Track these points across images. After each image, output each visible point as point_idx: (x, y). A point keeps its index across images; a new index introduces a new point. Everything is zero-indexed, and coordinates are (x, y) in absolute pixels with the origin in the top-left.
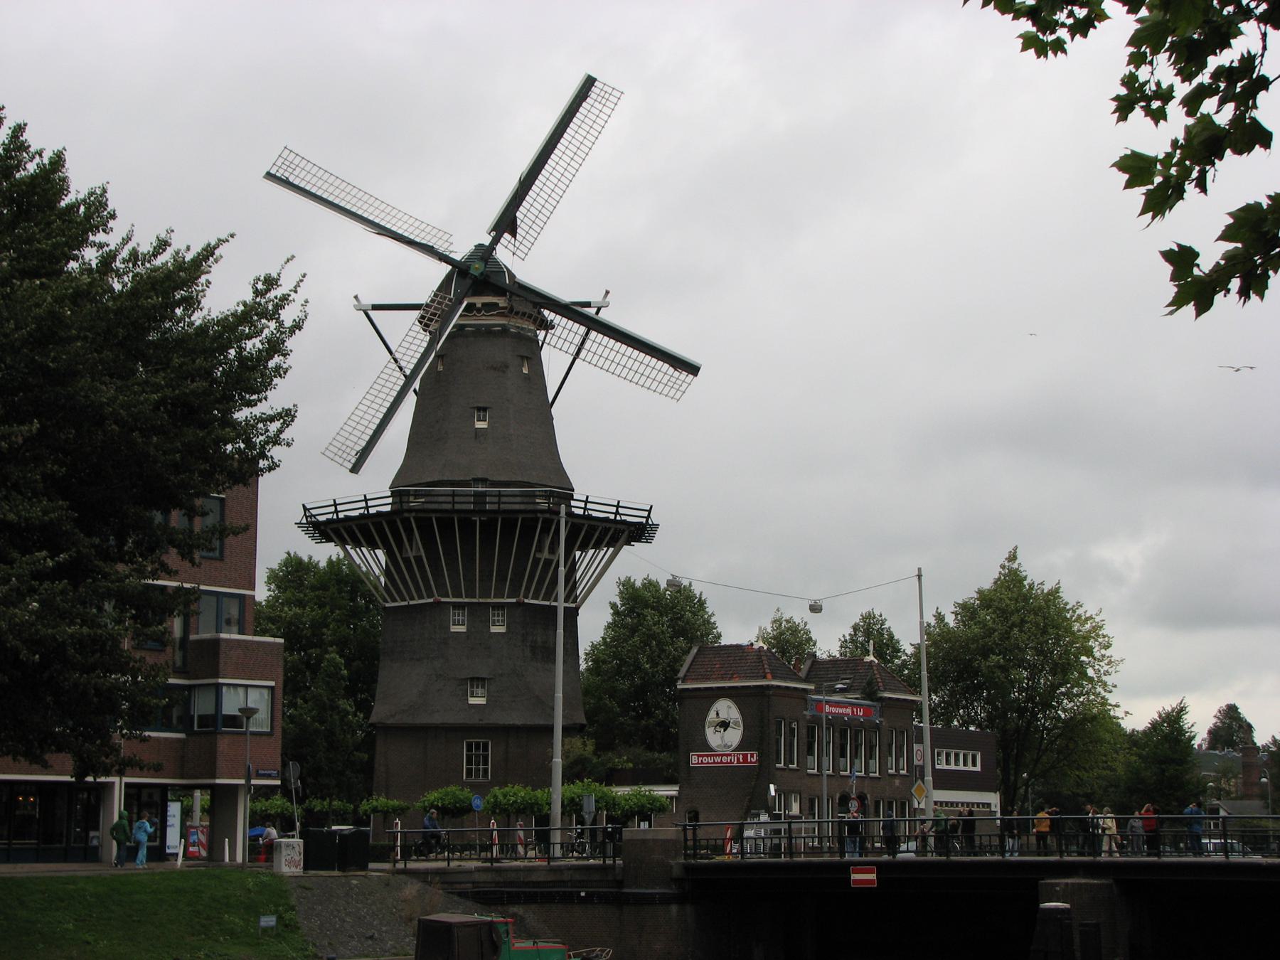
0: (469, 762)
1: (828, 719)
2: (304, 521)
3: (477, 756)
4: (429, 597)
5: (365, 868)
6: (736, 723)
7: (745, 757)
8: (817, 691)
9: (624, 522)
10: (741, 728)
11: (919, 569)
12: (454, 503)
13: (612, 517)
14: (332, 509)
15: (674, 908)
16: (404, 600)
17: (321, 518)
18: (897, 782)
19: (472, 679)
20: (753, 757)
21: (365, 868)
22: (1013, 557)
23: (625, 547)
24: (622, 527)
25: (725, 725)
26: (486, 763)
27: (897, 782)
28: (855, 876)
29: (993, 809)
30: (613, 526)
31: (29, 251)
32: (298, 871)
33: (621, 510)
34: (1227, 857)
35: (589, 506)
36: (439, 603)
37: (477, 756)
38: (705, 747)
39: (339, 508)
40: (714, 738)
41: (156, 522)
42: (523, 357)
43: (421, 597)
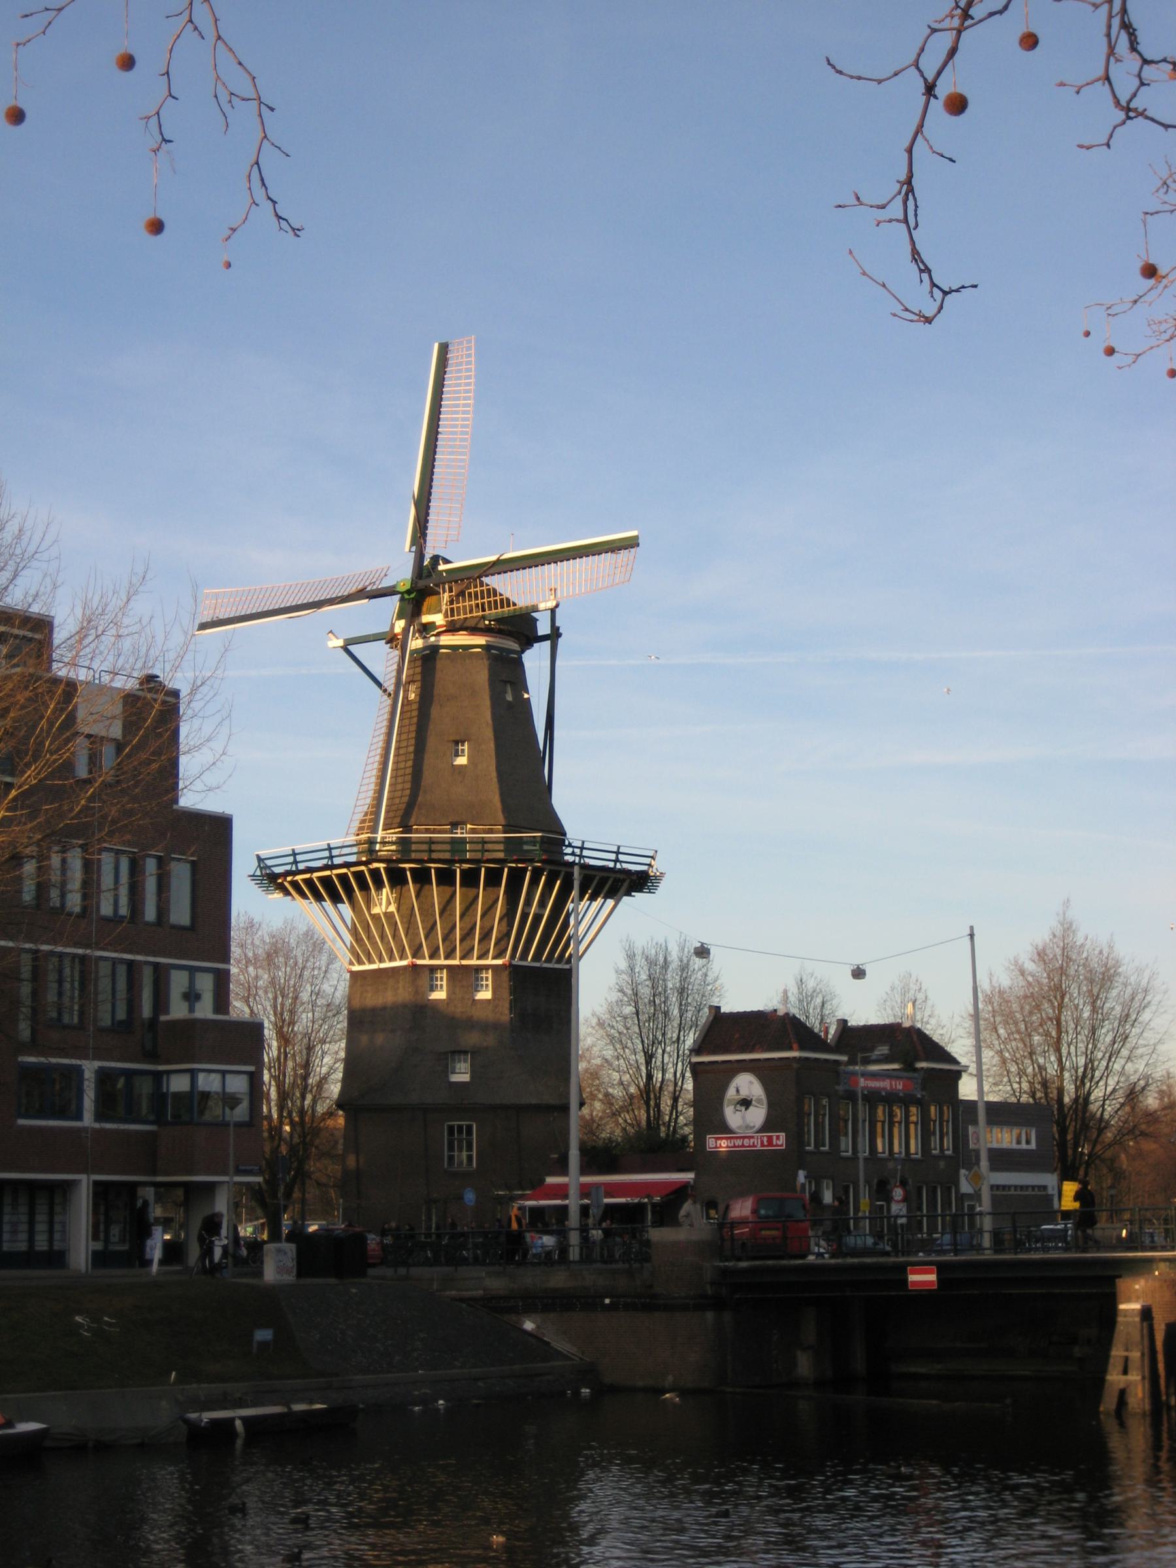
0: (451, 1148)
1: (863, 1095)
2: (258, 873)
3: (460, 1141)
4: (401, 959)
5: (364, 1275)
6: (759, 1101)
7: (770, 1139)
8: (852, 1062)
9: (628, 872)
10: (765, 1106)
11: (972, 928)
12: (431, 851)
13: (611, 865)
14: (291, 859)
15: (710, 1315)
16: (371, 961)
17: (277, 870)
18: (942, 1164)
19: (453, 1052)
20: (780, 1140)
21: (364, 1275)
22: (1067, 903)
23: (625, 898)
24: (621, 876)
25: (746, 1103)
26: (470, 1148)
27: (942, 1164)
28: (913, 1278)
29: (1050, 1191)
30: (614, 875)
31: (1006, 1023)
32: (290, 1278)
33: (621, 857)
34: (191, 1010)
35: (585, 853)
36: (414, 966)
37: (460, 1141)
38: (723, 1128)
39: (299, 858)
40: (733, 1118)
41: (837, 1087)
42: (506, 682)
43: (391, 958)
